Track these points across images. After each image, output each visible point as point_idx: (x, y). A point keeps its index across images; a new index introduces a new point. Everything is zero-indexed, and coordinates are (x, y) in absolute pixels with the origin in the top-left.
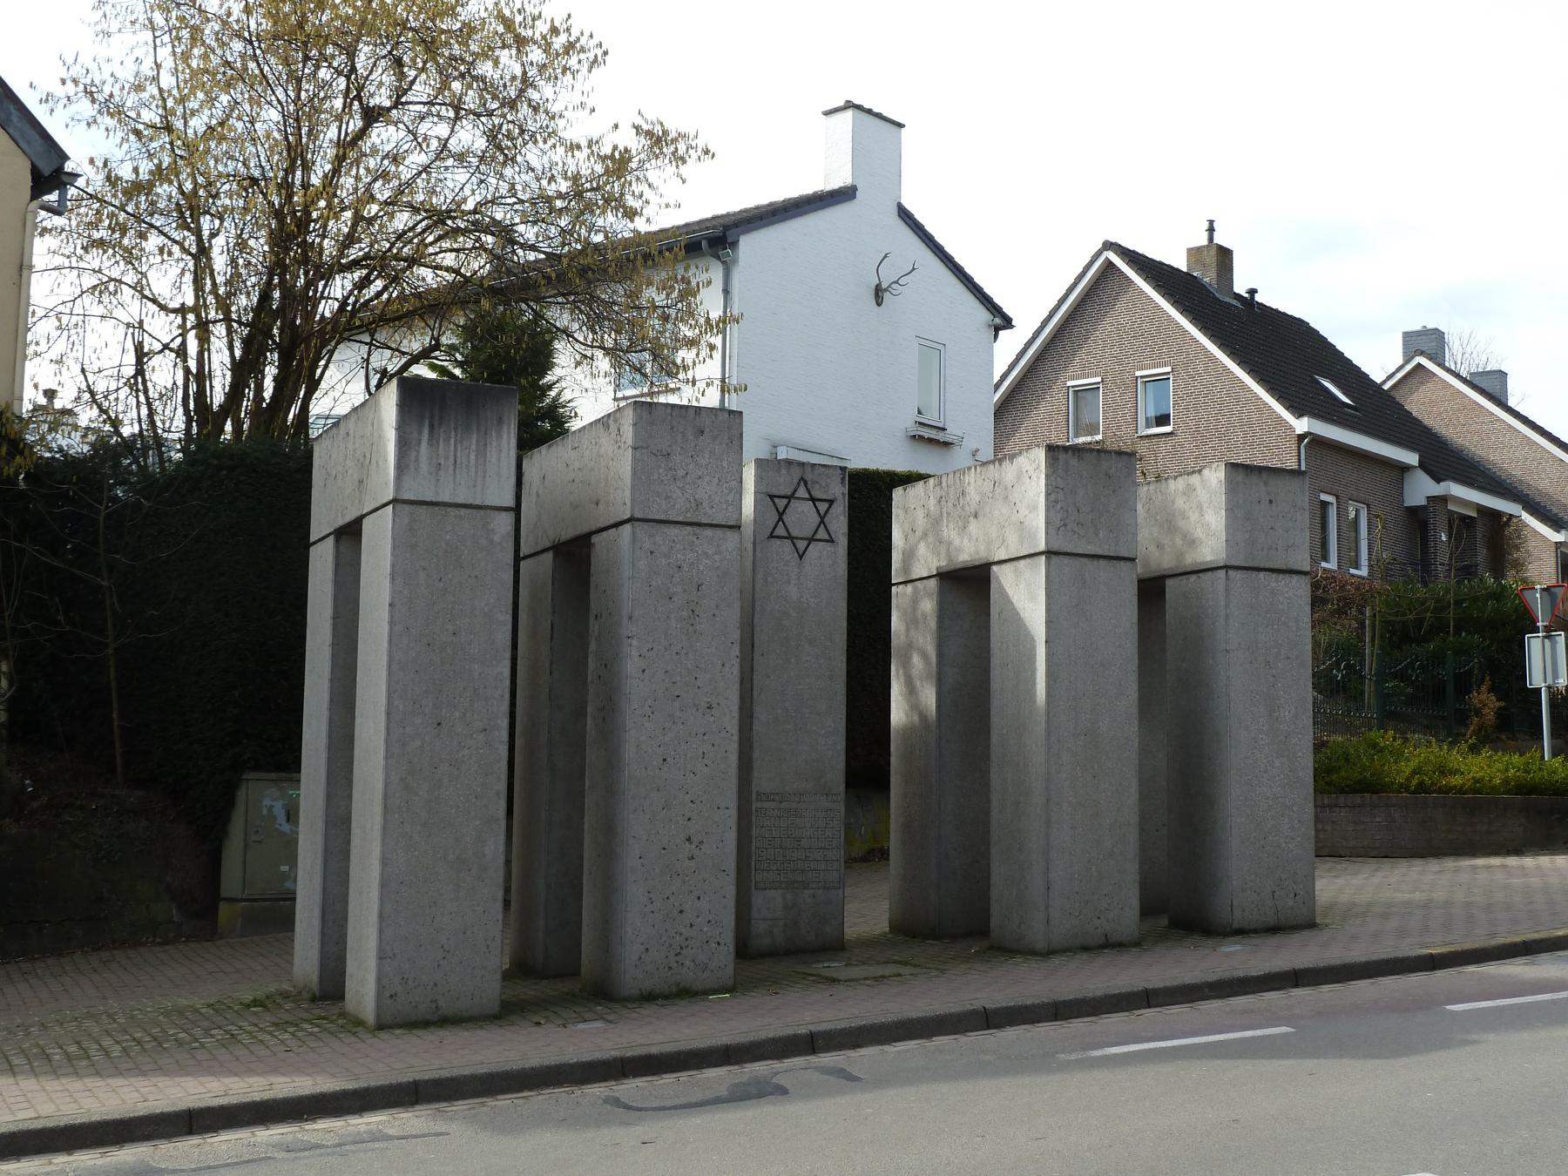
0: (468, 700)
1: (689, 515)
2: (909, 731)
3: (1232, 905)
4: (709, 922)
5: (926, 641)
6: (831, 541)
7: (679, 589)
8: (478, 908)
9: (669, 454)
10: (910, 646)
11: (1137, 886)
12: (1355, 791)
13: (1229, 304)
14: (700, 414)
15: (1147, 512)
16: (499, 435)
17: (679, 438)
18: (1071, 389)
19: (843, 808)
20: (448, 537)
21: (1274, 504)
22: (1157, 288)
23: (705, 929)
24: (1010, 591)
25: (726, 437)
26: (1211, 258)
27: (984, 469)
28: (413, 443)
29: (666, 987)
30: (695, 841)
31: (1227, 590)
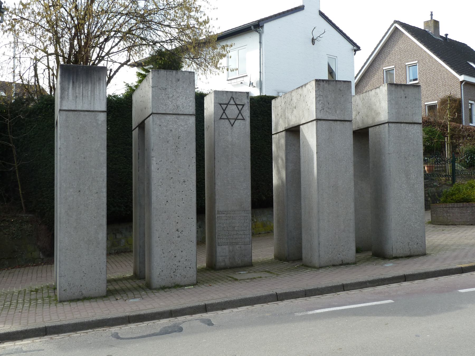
0: (90, 182)
1: (174, 111)
2: (278, 186)
3: (392, 248)
4: (186, 260)
5: (282, 154)
6: (244, 119)
7: (171, 139)
8: (97, 258)
9: (166, 89)
10: (278, 156)
11: (354, 242)
12: (460, 202)
13: (438, 39)
14: (178, 73)
15: (363, 104)
16: (99, 84)
17: (170, 82)
18: (385, 70)
19: (250, 215)
20: (81, 123)
21: (407, 98)
22: (412, 35)
23: (185, 263)
24: (306, 135)
25: (188, 82)
26: (432, 25)
27: (297, 90)
28: (66, 89)
29: (170, 284)
30: (180, 230)
31: (389, 131)
